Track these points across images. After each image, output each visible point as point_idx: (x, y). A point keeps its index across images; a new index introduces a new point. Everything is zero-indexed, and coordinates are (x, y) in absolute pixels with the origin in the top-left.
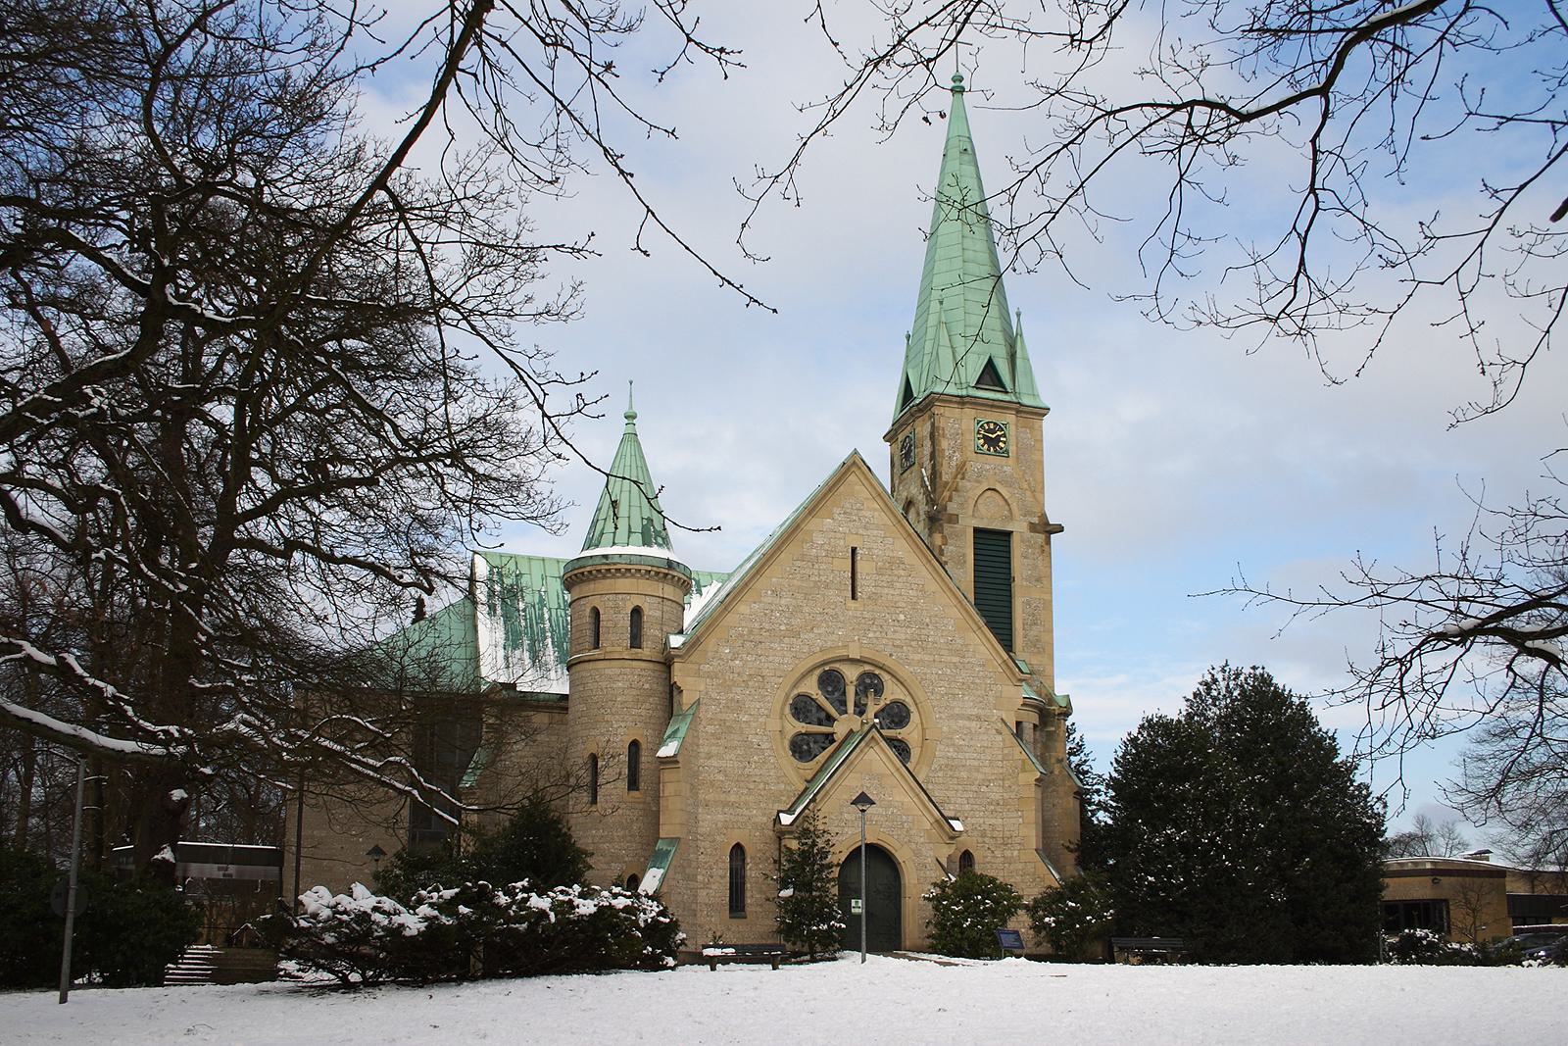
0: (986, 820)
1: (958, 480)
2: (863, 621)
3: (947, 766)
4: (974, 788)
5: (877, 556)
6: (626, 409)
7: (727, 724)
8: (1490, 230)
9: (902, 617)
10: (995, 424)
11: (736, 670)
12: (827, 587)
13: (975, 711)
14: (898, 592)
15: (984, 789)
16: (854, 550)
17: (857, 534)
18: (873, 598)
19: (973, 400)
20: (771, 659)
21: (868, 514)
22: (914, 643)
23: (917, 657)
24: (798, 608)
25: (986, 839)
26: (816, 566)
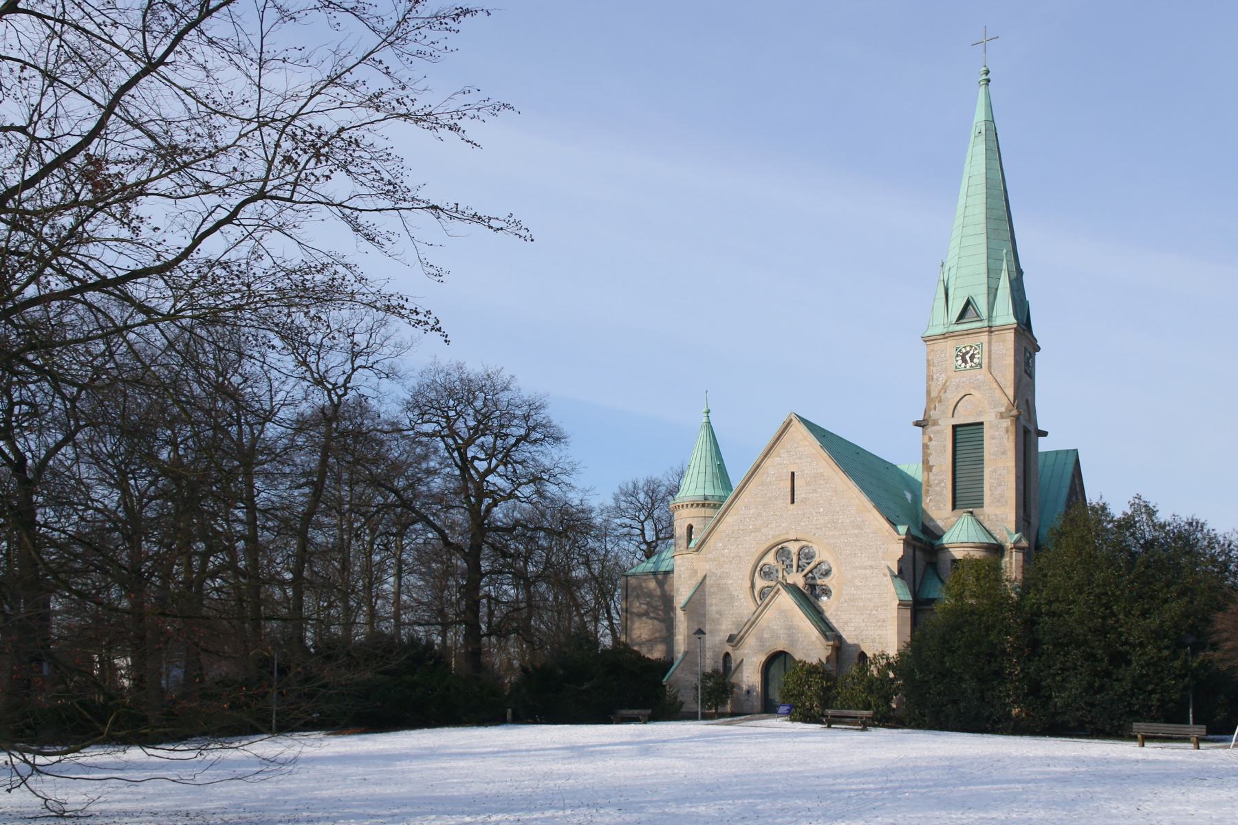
6: (705, 410)
8: (262, 38)
9: (822, 510)
10: (971, 347)
12: (776, 499)
15: (874, 612)
16: (793, 474)
18: (804, 501)
19: (951, 334)
22: (829, 525)
23: (831, 533)
25: (875, 644)
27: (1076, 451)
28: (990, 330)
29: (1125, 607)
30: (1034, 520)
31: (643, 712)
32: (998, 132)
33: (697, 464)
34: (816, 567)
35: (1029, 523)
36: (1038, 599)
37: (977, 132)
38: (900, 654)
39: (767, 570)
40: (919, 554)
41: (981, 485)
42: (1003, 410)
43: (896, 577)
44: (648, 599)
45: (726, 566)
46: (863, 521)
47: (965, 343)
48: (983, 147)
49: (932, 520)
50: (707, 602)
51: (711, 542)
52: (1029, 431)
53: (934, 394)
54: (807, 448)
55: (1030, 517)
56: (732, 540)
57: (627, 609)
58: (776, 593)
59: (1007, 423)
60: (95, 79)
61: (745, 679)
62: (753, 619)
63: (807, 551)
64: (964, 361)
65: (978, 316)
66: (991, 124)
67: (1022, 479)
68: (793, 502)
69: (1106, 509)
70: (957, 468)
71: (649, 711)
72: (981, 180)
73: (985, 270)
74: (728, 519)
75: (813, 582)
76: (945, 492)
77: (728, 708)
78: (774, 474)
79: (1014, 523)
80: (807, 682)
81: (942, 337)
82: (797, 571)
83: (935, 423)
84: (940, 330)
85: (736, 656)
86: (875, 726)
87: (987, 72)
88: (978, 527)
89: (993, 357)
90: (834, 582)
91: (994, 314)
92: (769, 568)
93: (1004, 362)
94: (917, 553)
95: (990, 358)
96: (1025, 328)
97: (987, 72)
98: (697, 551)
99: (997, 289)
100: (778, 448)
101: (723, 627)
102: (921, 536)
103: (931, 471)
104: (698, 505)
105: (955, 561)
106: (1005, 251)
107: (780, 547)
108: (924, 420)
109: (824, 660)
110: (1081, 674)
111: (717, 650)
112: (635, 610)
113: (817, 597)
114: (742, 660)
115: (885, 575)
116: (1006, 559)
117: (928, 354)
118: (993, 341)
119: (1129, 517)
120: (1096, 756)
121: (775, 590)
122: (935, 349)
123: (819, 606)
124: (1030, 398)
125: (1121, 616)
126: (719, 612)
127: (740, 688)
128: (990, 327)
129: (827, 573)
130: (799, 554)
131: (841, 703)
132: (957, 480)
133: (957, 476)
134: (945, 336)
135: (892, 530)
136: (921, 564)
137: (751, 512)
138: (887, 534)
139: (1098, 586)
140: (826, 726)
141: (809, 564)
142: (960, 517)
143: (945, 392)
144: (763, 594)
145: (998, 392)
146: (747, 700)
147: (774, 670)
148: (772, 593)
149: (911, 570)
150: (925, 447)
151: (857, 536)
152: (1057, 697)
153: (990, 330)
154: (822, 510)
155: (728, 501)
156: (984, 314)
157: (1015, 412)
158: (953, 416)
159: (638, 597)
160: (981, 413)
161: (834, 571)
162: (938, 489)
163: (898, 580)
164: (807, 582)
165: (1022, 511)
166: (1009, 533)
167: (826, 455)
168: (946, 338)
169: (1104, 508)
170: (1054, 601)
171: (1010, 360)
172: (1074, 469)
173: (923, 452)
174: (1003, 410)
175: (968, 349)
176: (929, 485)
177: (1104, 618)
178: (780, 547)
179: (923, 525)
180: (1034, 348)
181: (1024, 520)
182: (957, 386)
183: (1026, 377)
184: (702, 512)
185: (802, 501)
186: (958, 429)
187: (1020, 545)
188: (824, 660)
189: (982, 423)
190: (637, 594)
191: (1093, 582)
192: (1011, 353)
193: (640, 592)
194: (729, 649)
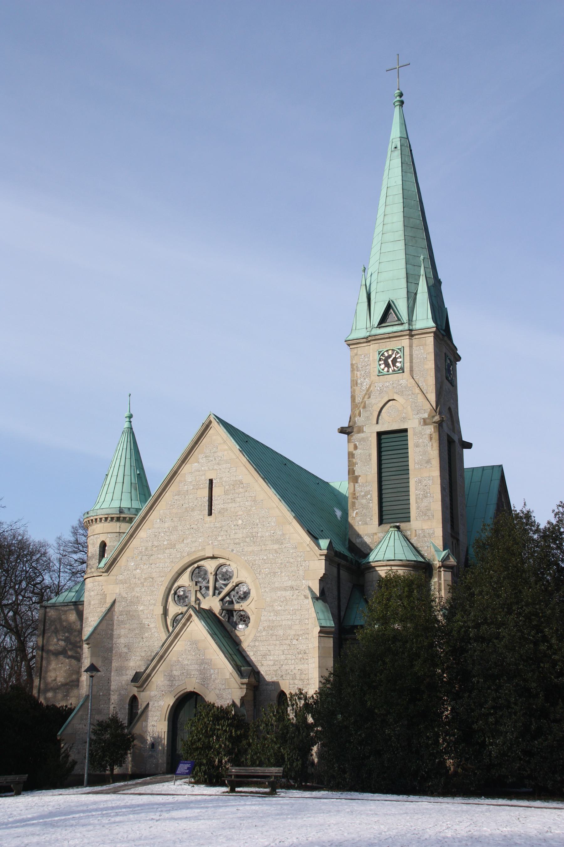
0: (296, 666)
1: (365, 399)
2: (215, 529)
3: (269, 627)
4: (288, 642)
5: (225, 482)
6: (127, 414)
7: (131, 613)
10: (392, 350)
11: (137, 576)
12: (193, 510)
13: (289, 583)
15: (295, 642)
16: (211, 481)
17: (213, 469)
19: (374, 338)
20: (157, 565)
21: (220, 454)
22: (248, 540)
23: (250, 549)
24: (175, 528)
25: (296, 682)
26: (187, 497)
27: (501, 466)
28: (411, 334)
29: (557, 630)
30: (462, 537)
31: (17, 778)
32: (412, 148)
33: (115, 473)
34: (233, 590)
35: (458, 540)
36: (465, 622)
37: (393, 147)
38: (321, 692)
39: (182, 593)
40: (344, 574)
41: (406, 498)
42: (426, 415)
43: (317, 599)
44: (67, 634)
45: (137, 589)
46: (283, 535)
47: (388, 346)
48: (399, 160)
49: (359, 536)
50: (115, 633)
51: (122, 561)
52: (454, 442)
53: (358, 400)
54: (226, 452)
55: (458, 533)
56: (144, 558)
57: (43, 646)
58: (188, 619)
59: (430, 429)
61: (150, 729)
62: (161, 653)
63: (224, 570)
64: (387, 365)
65: (399, 320)
66: (405, 140)
67: (447, 490)
68: (210, 514)
69: (530, 516)
70: (383, 479)
71: (25, 777)
72: (398, 190)
73: (404, 275)
74: (142, 534)
75: (230, 607)
76: (371, 505)
77: (129, 765)
78: (191, 482)
79: (441, 538)
80: (213, 730)
81: (365, 340)
82: (214, 594)
83: (360, 430)
84: (363, 333)
85: (143, 698)
86: (289, 787)
87: (401, 95)
88: (404, 543)
89: (414, 361)
90: (252, 606)
91: (414, 318)
92: (184, 591)
93: (425, 366)
94: (342, 572)
95: (411, 361)
96: (444, 334)
97: (401, 95)
98: (107, 571)
99: (416, 294)
100: (197, 454)
101: (131, 664)
102: (347, 553)
103: (357, 482)
104: (112, 519)
105: (380, 579)
106: (422, 257)
107: (196, 565)
108: (349, 427)
109: (238, 703)
110: (515, 713)
111: (122, 692)
112: (52, 648)
113: (235, 625)
114: (148, 704)
115: (306, 597)
116: (435, 580)
117: (352, 358)
118: (414, 345)
119: (554, 527)
120: (533, 833)
121: (186, 616)
122: (359, 353)
123: (237, 636)
124: (452, 407)
125: (553, 641)
126: (128, 646)
127: (143, 739)
128: (411, 330)
129: (246, 596)
130: (216, 574)
131: (252, 757)
132: (384, 492)
133: (383, 487)
134: (368, 340)
135: (313, 544)
136: (346, 587)
137: (166, 525)
138: (308, 549)
139: (527, 605)
140: (227, 789)
142: (387, 532)
143: (369, 397)
144: (175, 620)
145: (420, 397)
146: (151, 756)
147: (183, 716)
148: (183, 621)
149: (335, 593)
150: (351, 455)
151: (276, 552)
152: (491, 744)
153: (411, 334)
155: (142, 513)
156: (405, 318)
157: (437, 418)
158: (377, 423)
159: (56, 632)
160: (404, 420)
161: (253, 594)
162: (364, 501)
163: (320, 603)
164: (224, 608)
165: (449, 526)
166: (437, 551)
167: (245, 460)
168: (369, 341)
169: (528, 516)
170: (482, 623)
171: (431, 365)
172: (500, 493)
173: (349, 461)
174: (426, 415)
175: (390, 352)
176: (355, 498)
177: (536, 644)
178: (196, 565)
179: (350, 541)
180: (455, 357)
181: (452, 536)
182: (381, 391)
183: (447, 385)
184: (115, 526)
185: (220, 512)
186: (383, 437)
187: (448, 563)
188: (238, 703)
189: (406, 431)
190: (56, 628)
191: (522, 600)
192: (432, 357)
193: (58, 626)
194: (135, 691)
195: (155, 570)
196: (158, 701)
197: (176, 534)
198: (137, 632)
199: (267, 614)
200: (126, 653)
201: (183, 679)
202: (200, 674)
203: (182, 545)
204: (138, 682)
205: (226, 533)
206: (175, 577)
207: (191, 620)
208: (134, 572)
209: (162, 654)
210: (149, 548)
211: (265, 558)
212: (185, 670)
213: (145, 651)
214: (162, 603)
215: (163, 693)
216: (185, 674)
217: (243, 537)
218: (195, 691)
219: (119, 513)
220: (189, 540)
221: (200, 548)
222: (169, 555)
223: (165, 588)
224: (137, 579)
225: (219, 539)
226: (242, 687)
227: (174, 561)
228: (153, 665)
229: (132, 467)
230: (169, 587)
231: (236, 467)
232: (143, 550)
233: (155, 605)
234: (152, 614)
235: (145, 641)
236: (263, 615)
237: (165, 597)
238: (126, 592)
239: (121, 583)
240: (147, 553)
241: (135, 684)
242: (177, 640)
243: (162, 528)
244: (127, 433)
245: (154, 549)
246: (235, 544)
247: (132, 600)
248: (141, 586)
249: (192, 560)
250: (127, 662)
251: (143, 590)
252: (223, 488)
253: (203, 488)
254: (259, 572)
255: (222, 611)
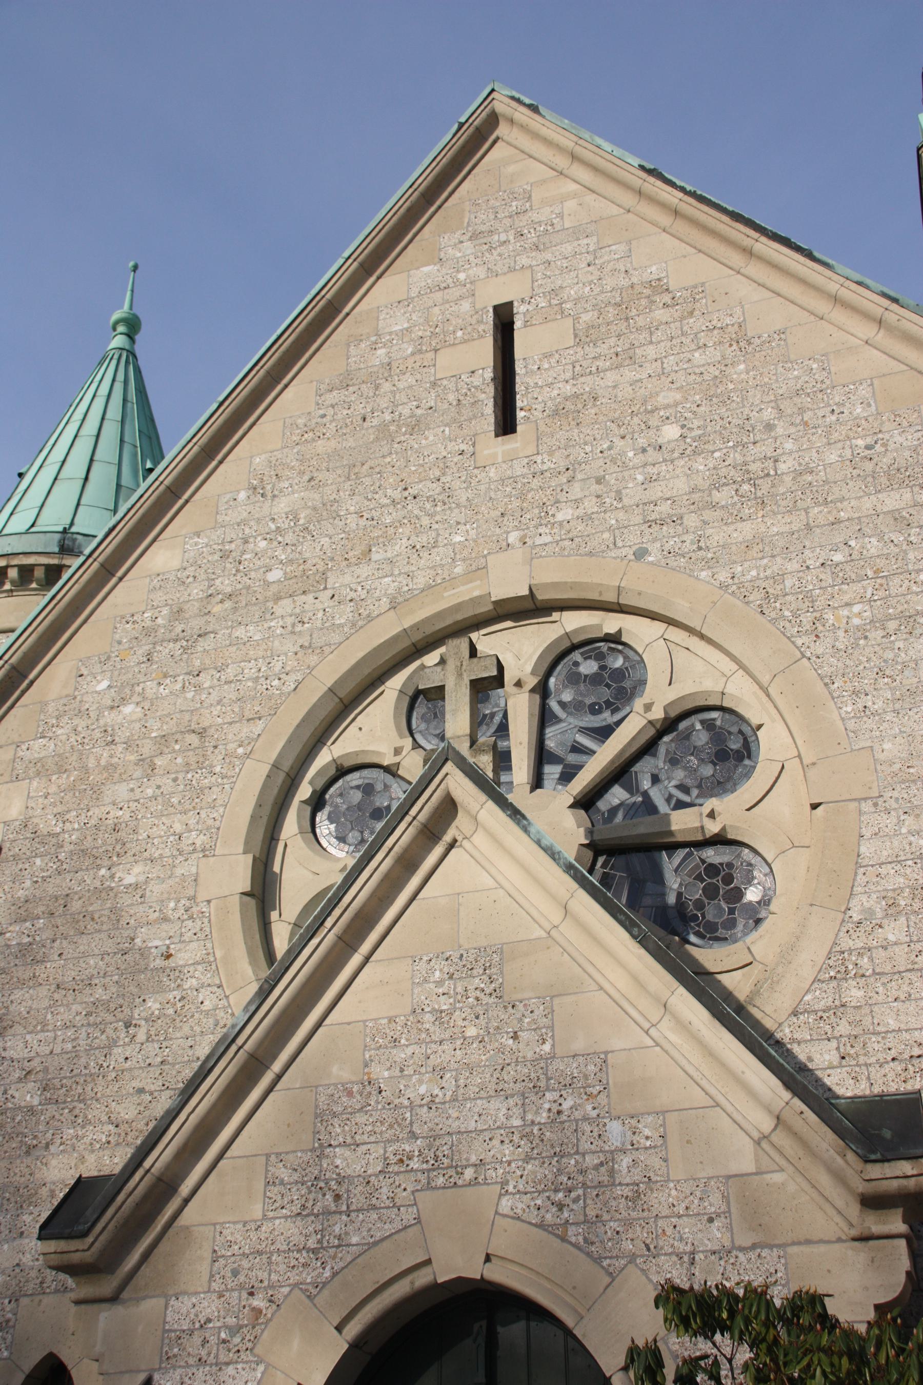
2: (535, 483)
5: (577, 301)
7: (76, 906)
12: (416, 426)
14: (649, 369)
17: (512, 270)
20: (231, 671)
26: (386, 386)
45: (121, 791)
60: (874, 950)
62: (251, 1040)
107: (611, 623)
137: (282, 505)
141: (604, 733)
154: (671, 432)
195: (214, 696)
196: (220, 1366)
197: (331, 531)
198: (99, 993)
199: (900, 822)
200: (31, 1110)
201: (403, 1197)
202: (527, 1159)
203: (364, 571)
204: (85, 1234)
205: (595, 488)
206: (323, 714)
207: (447, 838)
208: (109, 718)
209: (261, 1043)
210: (192, 608)
211: (838, 557)
212: (413, 1136)
213: (141, 1091)
214: (247, 843)
215: (258, 1302)
216: (415, 1164)
217: (694, 490)
218: (497, 1274)
219: (56, 550)
220: (400, 547)
221: (459, 570)
222: (289, 621)
223: (265, 769)
224: (120, 748)
225: (560, 517)
226: (876, 1229)
227: (318, 641)
228: (194, 1120)
229: (127, 449)
230: (287, 765)
231: (629, 242)
232: (160, 621)
233: (206, 852)
234: (192, 898)
235: (141, 1036)
236: (867, 833)
237: (267, 810)
238: (59, 809)
239: (38, 774)
240: (179, 629)
241: (62, 1245)
242: (356, 960)
243: (258, 521)
244: (114, 362)
245: (217, 609)
246: (650, 523)
247: (89, 843)
248: (138, 774)
249: (416, 627)
250: (28, 1160)
251: (150, 792)
252: (569, 322)
253: (465, 341)
254: (807, 626)
255: (589, 854)
